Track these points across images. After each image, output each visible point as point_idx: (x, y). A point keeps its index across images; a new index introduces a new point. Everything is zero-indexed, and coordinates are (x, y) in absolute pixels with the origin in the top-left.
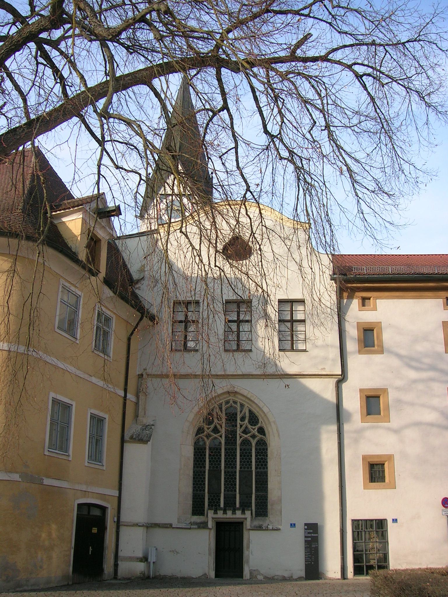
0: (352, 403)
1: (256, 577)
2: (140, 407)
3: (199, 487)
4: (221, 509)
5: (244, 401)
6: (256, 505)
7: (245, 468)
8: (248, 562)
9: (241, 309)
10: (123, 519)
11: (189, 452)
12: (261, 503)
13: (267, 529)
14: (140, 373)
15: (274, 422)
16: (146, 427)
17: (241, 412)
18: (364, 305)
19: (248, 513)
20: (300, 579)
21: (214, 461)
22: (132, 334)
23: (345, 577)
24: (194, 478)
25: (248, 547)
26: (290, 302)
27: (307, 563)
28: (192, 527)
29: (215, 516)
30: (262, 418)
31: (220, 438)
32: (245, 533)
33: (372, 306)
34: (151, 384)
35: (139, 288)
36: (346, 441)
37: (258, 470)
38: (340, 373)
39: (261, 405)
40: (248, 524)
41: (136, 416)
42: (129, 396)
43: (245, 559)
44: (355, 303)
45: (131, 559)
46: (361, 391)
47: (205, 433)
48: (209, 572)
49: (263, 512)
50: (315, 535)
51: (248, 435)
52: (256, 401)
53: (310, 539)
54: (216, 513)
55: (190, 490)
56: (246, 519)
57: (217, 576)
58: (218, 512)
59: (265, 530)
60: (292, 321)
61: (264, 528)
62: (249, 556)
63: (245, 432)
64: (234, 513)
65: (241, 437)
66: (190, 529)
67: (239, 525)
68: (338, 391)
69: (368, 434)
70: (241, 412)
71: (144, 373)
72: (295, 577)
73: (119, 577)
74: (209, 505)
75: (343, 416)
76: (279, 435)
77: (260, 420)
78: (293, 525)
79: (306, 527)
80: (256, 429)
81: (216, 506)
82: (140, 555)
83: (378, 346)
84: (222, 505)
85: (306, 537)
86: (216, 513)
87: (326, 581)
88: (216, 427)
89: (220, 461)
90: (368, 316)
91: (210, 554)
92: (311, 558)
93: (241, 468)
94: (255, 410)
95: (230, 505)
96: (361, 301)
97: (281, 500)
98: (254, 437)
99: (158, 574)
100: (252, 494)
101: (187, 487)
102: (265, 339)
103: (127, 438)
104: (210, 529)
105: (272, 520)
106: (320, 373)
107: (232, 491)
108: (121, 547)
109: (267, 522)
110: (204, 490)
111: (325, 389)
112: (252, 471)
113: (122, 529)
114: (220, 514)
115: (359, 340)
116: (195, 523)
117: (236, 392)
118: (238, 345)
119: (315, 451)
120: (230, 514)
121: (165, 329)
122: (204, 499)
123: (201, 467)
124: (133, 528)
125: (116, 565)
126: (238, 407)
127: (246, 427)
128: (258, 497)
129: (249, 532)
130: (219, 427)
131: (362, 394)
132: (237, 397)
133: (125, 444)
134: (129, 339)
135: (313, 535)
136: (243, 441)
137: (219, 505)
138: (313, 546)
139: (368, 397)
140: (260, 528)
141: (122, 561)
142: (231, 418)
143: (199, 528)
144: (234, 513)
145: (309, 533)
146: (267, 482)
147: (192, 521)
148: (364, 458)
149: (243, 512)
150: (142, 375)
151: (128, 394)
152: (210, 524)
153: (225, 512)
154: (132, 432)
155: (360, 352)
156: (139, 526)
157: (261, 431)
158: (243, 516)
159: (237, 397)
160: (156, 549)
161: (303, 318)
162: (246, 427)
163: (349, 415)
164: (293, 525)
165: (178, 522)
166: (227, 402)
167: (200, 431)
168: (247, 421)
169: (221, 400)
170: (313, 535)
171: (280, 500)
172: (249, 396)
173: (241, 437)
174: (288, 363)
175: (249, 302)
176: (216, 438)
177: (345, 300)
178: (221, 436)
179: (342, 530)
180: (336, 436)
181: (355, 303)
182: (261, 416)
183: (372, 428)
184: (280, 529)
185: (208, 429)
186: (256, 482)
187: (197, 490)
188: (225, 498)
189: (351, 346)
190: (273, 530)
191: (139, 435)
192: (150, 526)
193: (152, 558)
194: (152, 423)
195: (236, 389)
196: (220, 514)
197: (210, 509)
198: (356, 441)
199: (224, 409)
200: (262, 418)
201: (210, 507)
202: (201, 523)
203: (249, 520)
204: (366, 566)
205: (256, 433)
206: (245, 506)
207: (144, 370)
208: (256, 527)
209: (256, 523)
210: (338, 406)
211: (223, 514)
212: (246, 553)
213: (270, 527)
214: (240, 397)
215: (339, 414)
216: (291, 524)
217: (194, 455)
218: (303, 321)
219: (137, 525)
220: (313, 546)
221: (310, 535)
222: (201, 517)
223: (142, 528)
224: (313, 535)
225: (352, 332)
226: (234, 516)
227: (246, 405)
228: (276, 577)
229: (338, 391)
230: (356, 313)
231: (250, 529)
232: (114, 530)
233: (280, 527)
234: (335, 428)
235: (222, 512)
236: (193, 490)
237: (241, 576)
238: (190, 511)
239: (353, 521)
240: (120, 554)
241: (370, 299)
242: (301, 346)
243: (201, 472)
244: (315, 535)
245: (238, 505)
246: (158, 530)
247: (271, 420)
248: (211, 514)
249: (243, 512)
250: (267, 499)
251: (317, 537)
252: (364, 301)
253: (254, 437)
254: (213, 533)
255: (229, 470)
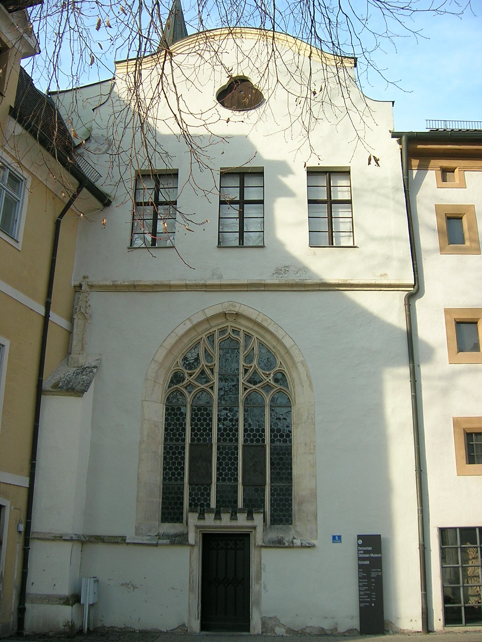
0: (433, 330)
1: (273, 630)
2: (75, 337)
3: (173, 474)
4: (211, 511)
5: (251, 329)
6: (272, 505)
7: (252, 441)
8: (258, 604)
9: (244, 182)
10: (37, 526)
11: (157, 414)
12: (281, 500)
13: (292, 546)
14: (77, 283)
15: (303, 363)
16: (83, 369)
17: (246, 347)
18: (444, 180)
19: (258, 519)
20: (350, 633)
21: (199, 430)
22: (62, 215)
23: (430, 629)
24: (165, 458)
25: (259, 578)
26: (325, 173)
27: (363, 605)
28: (160, 541)
29: (201, 523)
30: (282, 357)
31: (210, 390)
32: (254, 553)
33: (457, 181)
34: (96, 300)
35: (81, 155)
36: (426, 395)
37: (277, 444)
38: (412, 282)
39: (280, 334)
40: (258, 537)
41: (68, 352)
42: (53, 317)
43: (252, 598)
44: (431, 176)
45: (49, 599)
46: (447, 311)
47: (186, 381)
48: (189, 621)
49: (284, 516)
50: (376, 555)
51: (259, 385)
52: (271, 328)
53: (368, 562)
54: (201, 517)
55: (158, 478)
56: (255, 528)
57: (204, 627)
58: (206, 515)
59: (289, 547)
60: (330, 202)
61: (287, 544)
62: (259, 592)
63: (252, 381)
64: (234, 517)
65: (245, 389)
66: (157, 545)
67: (240, 542)
68: (409, 311)
69: (464, 381)
70: (246, 347)
71: (84, 284)
72: (341, 629)
73: (26, 633)
74: (190, 505)
75: (419, 352)
76: (311, 385)
77: (279, 360)
78: (336, 539)
79: (360, 542)
80: (272, 375)
81: (202, 505)
82: (65, 591)
83: (471, 240)
84: (213, 505)
85: (360, 559)
86: (201, 517)
87: (397, 636)
88: (203, 372)
89: (211, 430)
90: (453, 196)
91: (191, 590)
92: (370, 596)
93: (245, 441)
94: (270, 342)
95: (227, 503)
96: (440, 173)
97: (316, 495)
98: (268, 387)
99: (99, 625)
100: (264, 485)
101: (153, 473)
102: (289, 221)
103: (47, 385)
104: (192, 546)
105: (299, 530)
106: (378, 282)
107: (230, 480)
108: (32, 577)
109: (292, 533)
110: (182, 479)
111: (388, 308)
112: (264, 447)
113: (36, 547)
114: (210, 520)
115: (440, 231)
116: (168, 536)
117: (237, 314)
118: (241, 238)
119: (375, 411)
120: (226, 520)
121: (122, 213)
122: (182, 493)
123: (177, 440)
124: (54, 543)
125: (21, 611)
126: (241, 339)
127: (255, 372)
128: (275, 490)
129: (260, 552)
130: (208, 372)
131: (448, 317)
132: (239, 324)
133: (43, 397)
134: (57, 224)
135: (372, 555)
136: (249, 394)
137: (209, 505)
138: (373, 575)
139: (459, 323)
140: (279, 544)
141: (32, 602)
142: (230, 347)
143: (173, 543)
144: (234, 517)
145: (365, 552)
146: (291, 464)
147: (161, 531)
148: (457, 422)
149: (250, 517)
150: (80, 286)
151: (51, 313)
152: (192, 537)
153: (218, 516)
154: (58, 377)
155: (442, 250)
156: (65, 540)
157: (281, 378)
158: (249, 523)
159: (239, 324)
160: (97, 581)
161: (347, 198)
162: (255, 372)
163: (430, 351)
164: (336, 539)
165: (137, 534)
166: (223, 331)
167: (177, 378)
168: (255, 362)
169: (211, 327)
170: (372, 555)
171: (314, 495)
172: (259, 320)
173: (245, 389)
174: (326, 266)
175: (259, 173)
176: (203, 390)
177: (415, 172)
178: (212, 388)
179: (424, 545)
180: (408, 385)
181: (431, 176)
182: (280, 354)
183: (470, 371)
184: (311, 546)
185: (190, 375)
186: (272, 464)
187: (170, 479)
188: (217, 492)
189: (429, 240)
190: (302, 546)
191: (69, 382)
192: (87, 541)
193: (87, 599)
194: (94, 364)
195: (237, 309)
196: (210, 520)
197: (191, 511)
198: (445, 392)
199: (217, 341)
200: (282, 357)
201: (193, 506)
202: (176, 535)
203: (260, 529)
204: (465, 607)
205: (272, 382)
206: (253, 506)
207: (84, 278)
208: (273, 542)
209: (273, 535)
210: (411, 335)
211: (215, 519)
212: (254, 587)
213: (297, 542)
214: (243, 322)
215: (412, 350)
216: (334, 537)
217: (166, 419)
218: (349, 202)
219: (60, 538)
220: (373, 575)
221: (367, 556)
222: (177, 525)
223: (68, 546)
224: (372, 555)
225: (428, 219)
226: (234, 523)
227: (255, 335)
228: (308, 631)
229: (409, 311)
230: (433, 192)
231: (262, 547)
232: (19, 547)
233: (314, 542)
234: (405, 371)
235: (212, 516)
236: (164, 479)
237: (247, 628)
238: (158, 515)
239: (443, 531)
240: (31, 590)
241: (453, 172)
242: (345, 242)
243: (177, 448)
244: (376, 555)
245: (240, 504)
246: (101, 548)
247: (297, 360)
248: (193, 519)
249: (250, 517)
250: (291, 495)
251: (381, 558)
252: (445, 172)
253: (268, 387)
254: (197, 553)
255: (225, 444)
